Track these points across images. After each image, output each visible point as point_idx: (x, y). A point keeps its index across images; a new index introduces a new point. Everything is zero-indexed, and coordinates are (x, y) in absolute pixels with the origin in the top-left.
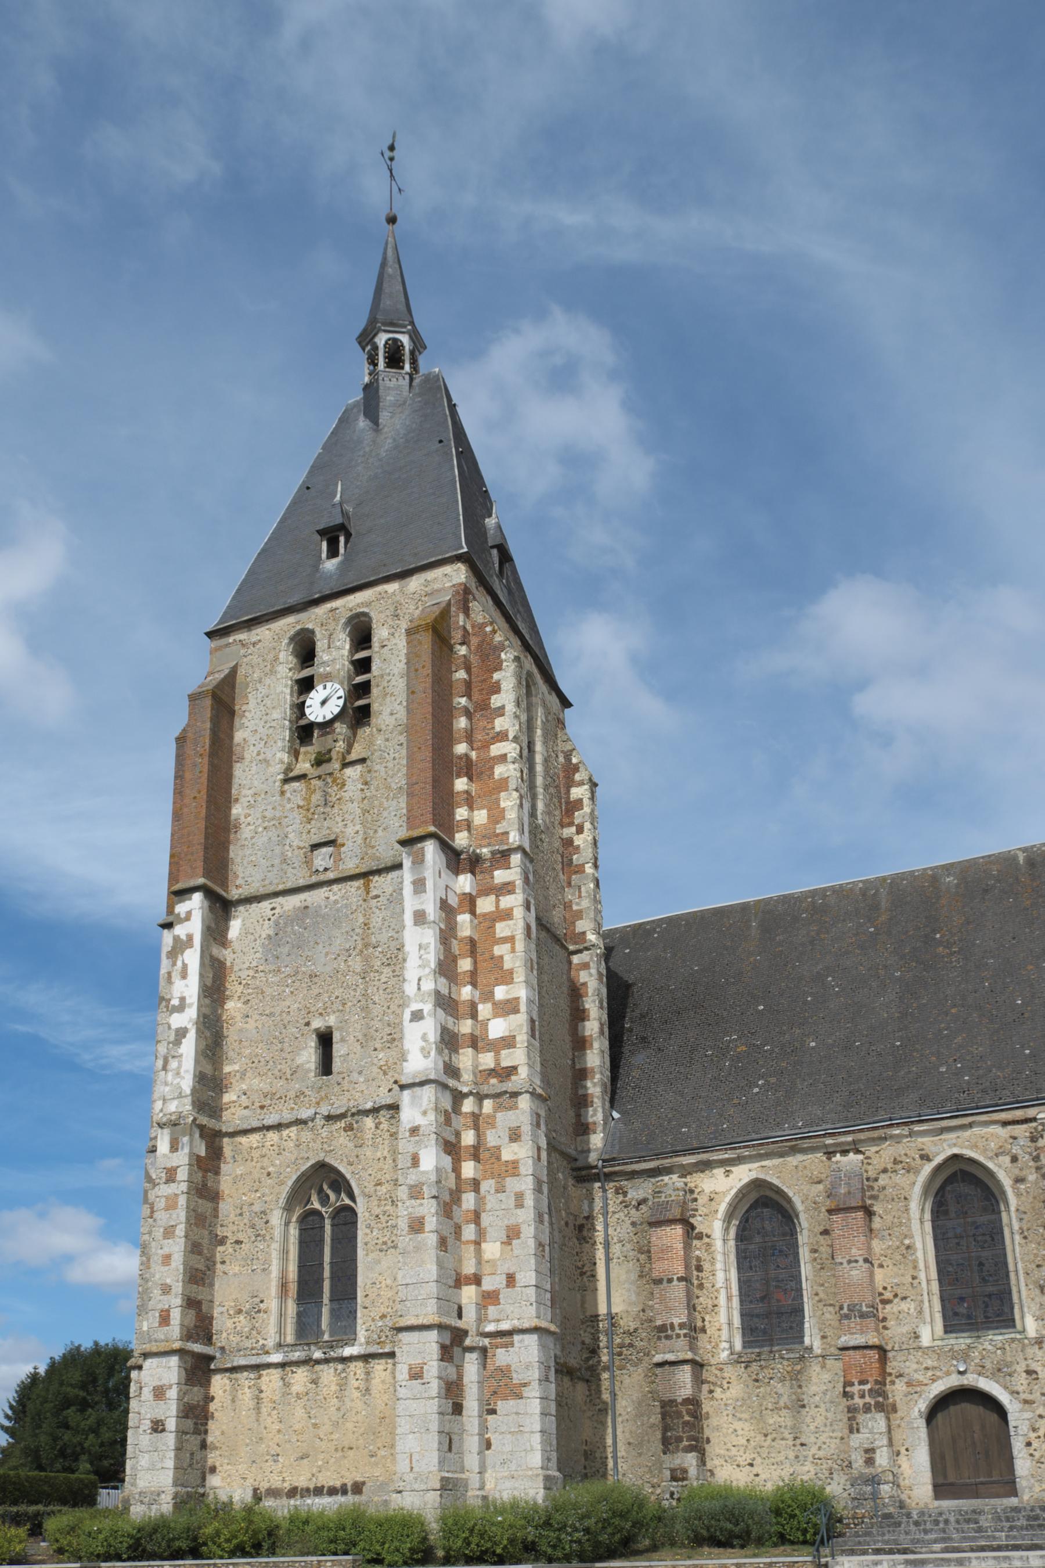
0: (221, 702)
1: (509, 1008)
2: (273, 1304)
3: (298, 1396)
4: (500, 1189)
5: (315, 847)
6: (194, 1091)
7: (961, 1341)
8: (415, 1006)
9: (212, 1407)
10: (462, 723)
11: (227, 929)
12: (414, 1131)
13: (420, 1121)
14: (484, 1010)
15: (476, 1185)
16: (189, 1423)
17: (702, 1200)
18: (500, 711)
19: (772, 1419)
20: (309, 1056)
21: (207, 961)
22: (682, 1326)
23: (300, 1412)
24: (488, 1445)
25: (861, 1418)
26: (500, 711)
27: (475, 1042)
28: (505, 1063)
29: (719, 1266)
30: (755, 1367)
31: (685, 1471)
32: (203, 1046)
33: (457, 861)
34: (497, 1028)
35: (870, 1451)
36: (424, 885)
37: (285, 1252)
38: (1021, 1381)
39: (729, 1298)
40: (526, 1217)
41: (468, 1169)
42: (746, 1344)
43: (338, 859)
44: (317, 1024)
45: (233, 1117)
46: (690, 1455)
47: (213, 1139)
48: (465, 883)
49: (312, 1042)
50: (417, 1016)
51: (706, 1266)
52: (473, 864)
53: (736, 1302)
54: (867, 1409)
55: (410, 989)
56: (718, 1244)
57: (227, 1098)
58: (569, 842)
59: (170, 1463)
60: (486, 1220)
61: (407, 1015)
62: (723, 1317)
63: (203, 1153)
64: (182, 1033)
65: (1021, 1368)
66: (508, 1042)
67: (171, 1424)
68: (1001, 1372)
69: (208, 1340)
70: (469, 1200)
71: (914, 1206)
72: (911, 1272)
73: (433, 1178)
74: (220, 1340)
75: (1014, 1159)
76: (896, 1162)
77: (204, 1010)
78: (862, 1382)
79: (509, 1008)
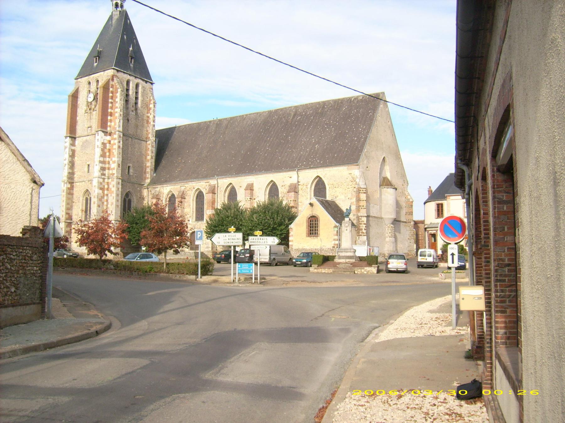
0: (74, 97)
1: (114, 162)
14: (111, 162)
15: (107, 195)
18: (117, 108)
20: (86, 169)
26: (117, 108)
27: (109, 169)
33: (106, 133)
36: (101, 137)
37: (83, 205)
40: (114, 201)
41: (106, 192)
43: (91, 130)
45: (76, 179)
46: (131, 133)
47: (72, 183)
48: (108, 138)
49: (87, 166)
52: (110, 134)
55: (96, 160)
58: (148, 117)
64: (65, 165)
66: (114, 169)
69: (71, 220)
70: (106, 198)
71: (118, 95)
74: (73, 220)
79: (114, 162)
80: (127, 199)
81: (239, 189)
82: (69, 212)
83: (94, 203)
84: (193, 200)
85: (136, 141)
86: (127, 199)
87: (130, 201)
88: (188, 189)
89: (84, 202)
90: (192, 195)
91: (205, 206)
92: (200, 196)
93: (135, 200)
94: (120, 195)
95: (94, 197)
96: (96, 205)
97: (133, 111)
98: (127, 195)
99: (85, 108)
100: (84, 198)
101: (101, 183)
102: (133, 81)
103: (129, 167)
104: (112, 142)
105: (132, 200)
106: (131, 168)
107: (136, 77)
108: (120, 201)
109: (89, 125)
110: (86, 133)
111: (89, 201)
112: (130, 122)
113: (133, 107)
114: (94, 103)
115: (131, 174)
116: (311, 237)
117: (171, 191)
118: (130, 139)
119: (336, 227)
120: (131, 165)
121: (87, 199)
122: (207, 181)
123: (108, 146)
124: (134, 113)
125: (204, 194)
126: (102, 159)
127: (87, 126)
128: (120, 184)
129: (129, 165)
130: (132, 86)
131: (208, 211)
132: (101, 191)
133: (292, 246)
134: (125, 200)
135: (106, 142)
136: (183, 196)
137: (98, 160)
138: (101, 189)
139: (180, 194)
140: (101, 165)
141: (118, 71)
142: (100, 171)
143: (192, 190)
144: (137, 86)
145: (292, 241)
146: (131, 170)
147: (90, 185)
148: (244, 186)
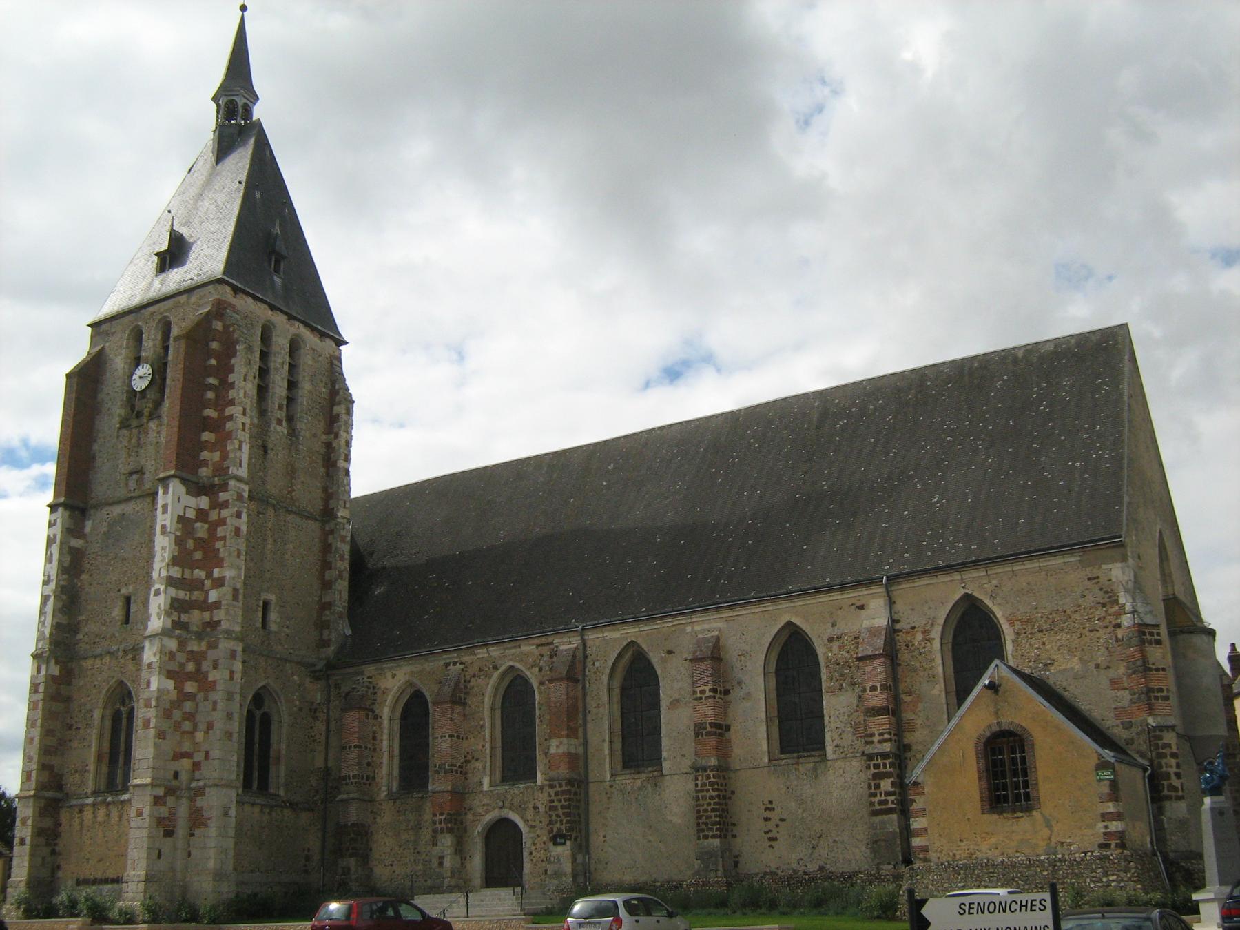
2: (92, 768)
3: (100, 824)
4: (206, 699)
5: (131, 473)
6: (51, 635)
7: (501, 789)
8: (157, 586)
9: (61, 829)
10: (210, 395)
11: (84, 527)
12: (150, 665)
13: (154, 659)
16: (42, 840)
17: (379, 693)
19: (405, 836)
20: (117, 613)
21: (66, 550)
22: (354, 777)
23: (100, 834)
24: (189, 855)
25: (439, 837)
28: (215, 619)
29: (385, 737)
30: (398, 802)
31: (349, 869)
32: (60, 604)
34: (213, 596)
35: (441, 858)
37: (101, 735)
38: (530, 813)
39: (391, 757)
42: (401, 787)
43: (140, 482)
44: (124, 591)
48: (204, 502)
50: (157, 593)
51: (378, 736)
53: (396, 761)
54: (442, 831)
55: (155, 575)
56: (386, 723)
57: (80, 636)
59: (26, 864)
60: (198, 717)
61: (152, 592)
62: (385, 770)
63: (57, 673)
65: (531, 806)
66: (217, 605)
67: (28, 840)
68: (521, 808)
72: (481, 743)
73: (155, 695)
75: (540, 670)
76: (481, 670)
77: (62, 583)
78: (441, 814)
80: (258, 714)
81: (663, 660)
82: (55, 761)
83: (146, 724)
84: (492, 709)
85: (291, 518)
86: (258, 714)
87: (266, 721)
88: (473, 670)
89: (108, 723)
90: (489, 691)
91: (540, 729)
92: (516, 695)
93: (285, 718)
94: (237, 698)
95: (148, 705)
96: (152, 732)
97: (279, 422)
98: (258, 699)
99: (122, 412)
100: (108, 712)
101: (172, 655)
102: (285, 331)
103: (266, 605)
104: (214, 516)
105: (275, 718)
106: (272, 607)
107: (291, 317)
108: (236, 716)
109: (132, 467)
110: (122, 493)
111: (124, 722)
112: (271, 454)
113: (280, 407)
114: (151, 395)
115: (274, 627)
116: (1001, 812)
117: (410, 684)
118: (271, 511)
119: (1103, 765)
120: (272, 597)
121: (116, 718)
122: (543, 640)
123: (201, 530)
124: (283, 429)
125: (535, 684)
126: (176, 572)
127: (123, 469)
128: (239, 657)
129: (264, 596)
130: (281, 343)
131: (554, 742)
132: (170, 684)
133: (925, 850)
134: (250, 717)
135: (191, 514)
136: (459, 697)
137: (164, 573)
138: (170, 675)
139: (447, 690)
140: (172, 592)
141: (236, 290)
142: (168, 614)
143: (488, 676)
144: (295, 346)
145: (923, 832)
146: (273, 616)
147: (131, 666)
148: (686, 647)
